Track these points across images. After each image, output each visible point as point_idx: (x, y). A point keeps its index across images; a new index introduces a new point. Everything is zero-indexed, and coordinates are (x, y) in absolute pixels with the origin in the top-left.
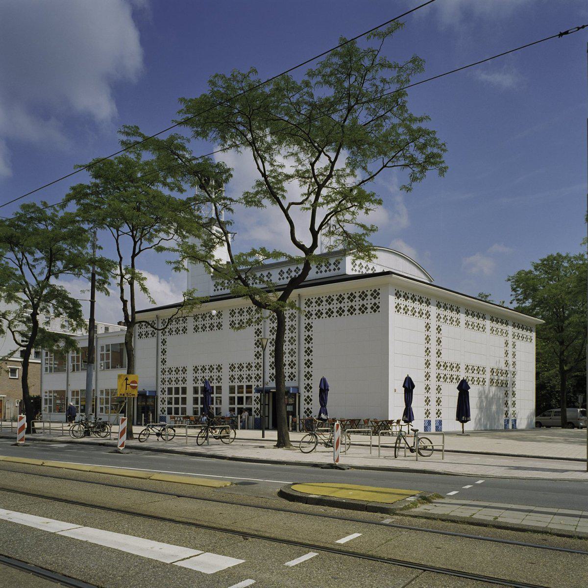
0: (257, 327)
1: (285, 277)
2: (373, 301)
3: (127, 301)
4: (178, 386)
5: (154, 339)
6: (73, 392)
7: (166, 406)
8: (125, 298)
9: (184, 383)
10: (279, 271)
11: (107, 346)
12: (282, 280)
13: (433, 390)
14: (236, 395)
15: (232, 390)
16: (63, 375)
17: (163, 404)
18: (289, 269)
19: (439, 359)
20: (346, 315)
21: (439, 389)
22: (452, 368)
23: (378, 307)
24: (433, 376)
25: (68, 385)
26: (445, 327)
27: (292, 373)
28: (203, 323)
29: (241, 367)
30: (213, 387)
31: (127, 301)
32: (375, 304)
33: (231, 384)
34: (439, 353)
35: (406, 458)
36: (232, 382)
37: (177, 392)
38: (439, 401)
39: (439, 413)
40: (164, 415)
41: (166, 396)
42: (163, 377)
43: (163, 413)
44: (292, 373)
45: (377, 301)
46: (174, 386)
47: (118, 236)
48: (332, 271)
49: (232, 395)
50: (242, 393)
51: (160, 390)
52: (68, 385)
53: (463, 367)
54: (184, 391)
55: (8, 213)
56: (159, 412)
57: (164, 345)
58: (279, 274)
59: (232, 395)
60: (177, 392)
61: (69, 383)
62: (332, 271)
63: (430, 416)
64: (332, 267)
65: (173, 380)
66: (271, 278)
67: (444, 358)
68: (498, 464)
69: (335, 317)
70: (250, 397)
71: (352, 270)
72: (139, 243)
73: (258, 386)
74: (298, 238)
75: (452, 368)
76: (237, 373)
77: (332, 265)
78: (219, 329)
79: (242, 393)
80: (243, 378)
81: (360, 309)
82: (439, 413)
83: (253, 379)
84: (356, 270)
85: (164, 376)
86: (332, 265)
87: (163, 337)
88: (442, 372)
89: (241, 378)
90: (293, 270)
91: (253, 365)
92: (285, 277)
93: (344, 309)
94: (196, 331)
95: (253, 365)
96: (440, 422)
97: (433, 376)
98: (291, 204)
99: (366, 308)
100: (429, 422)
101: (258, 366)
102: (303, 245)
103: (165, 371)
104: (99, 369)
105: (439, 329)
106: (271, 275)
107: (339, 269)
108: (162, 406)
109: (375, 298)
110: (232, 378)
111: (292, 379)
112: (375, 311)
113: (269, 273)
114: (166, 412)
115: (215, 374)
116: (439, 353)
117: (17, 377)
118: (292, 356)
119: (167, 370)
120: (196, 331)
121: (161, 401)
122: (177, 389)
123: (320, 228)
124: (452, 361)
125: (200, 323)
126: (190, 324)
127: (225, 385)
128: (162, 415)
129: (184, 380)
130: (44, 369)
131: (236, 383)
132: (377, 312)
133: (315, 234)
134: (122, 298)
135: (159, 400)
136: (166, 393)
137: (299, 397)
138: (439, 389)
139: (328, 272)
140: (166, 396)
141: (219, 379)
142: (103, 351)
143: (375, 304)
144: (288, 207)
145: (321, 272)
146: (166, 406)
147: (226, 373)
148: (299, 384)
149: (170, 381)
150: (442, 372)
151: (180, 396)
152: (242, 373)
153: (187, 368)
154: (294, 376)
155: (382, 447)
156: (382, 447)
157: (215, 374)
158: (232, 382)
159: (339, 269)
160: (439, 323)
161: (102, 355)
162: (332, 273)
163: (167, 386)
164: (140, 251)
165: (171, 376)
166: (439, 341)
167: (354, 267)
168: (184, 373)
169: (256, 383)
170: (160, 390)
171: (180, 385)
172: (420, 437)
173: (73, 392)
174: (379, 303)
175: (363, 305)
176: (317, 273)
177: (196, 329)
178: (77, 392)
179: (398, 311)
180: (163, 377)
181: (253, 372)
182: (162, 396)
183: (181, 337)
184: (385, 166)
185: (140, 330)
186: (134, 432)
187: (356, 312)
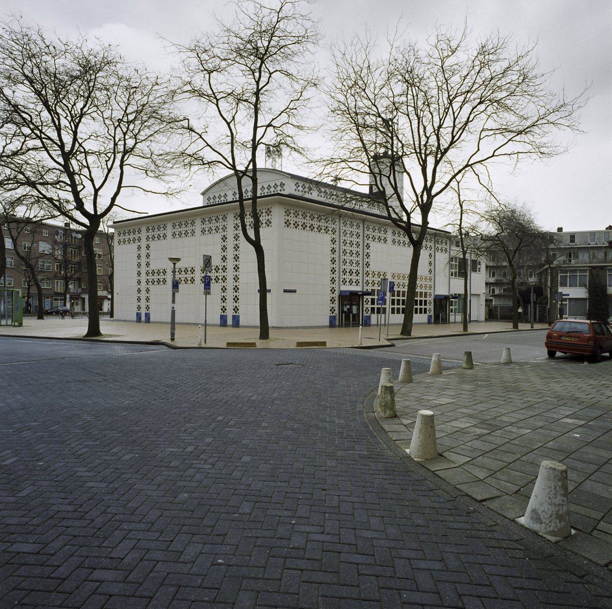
21: (148, 291)
28: (153, 233)
34: (148, 264)
41: (428, 307)
42: (358, 278)
66: (227, 198)
67: (153, 267)
68: (477, 336)
71: (296, 190)
78: (268, 226)
82: (148, 308)
84: (299, 190)
91: (220, 268)
95: (220, 268)
103: (222, 279)
106: (284, 185)
107: (284, 190)
116: (148, 264)
122: (426, 293)
124: (399, 248)
126: (169, 231)
136: (370, 303)
138: (148, 291)
140: (428, 307)
150: (151, 277)
151: (396, 306)
165: (153, 277)
166: (148, 256)
167: (297, 188)
168: (224, 282)
172: (383, 322)
180: (358, 278)
183: (162, 242)
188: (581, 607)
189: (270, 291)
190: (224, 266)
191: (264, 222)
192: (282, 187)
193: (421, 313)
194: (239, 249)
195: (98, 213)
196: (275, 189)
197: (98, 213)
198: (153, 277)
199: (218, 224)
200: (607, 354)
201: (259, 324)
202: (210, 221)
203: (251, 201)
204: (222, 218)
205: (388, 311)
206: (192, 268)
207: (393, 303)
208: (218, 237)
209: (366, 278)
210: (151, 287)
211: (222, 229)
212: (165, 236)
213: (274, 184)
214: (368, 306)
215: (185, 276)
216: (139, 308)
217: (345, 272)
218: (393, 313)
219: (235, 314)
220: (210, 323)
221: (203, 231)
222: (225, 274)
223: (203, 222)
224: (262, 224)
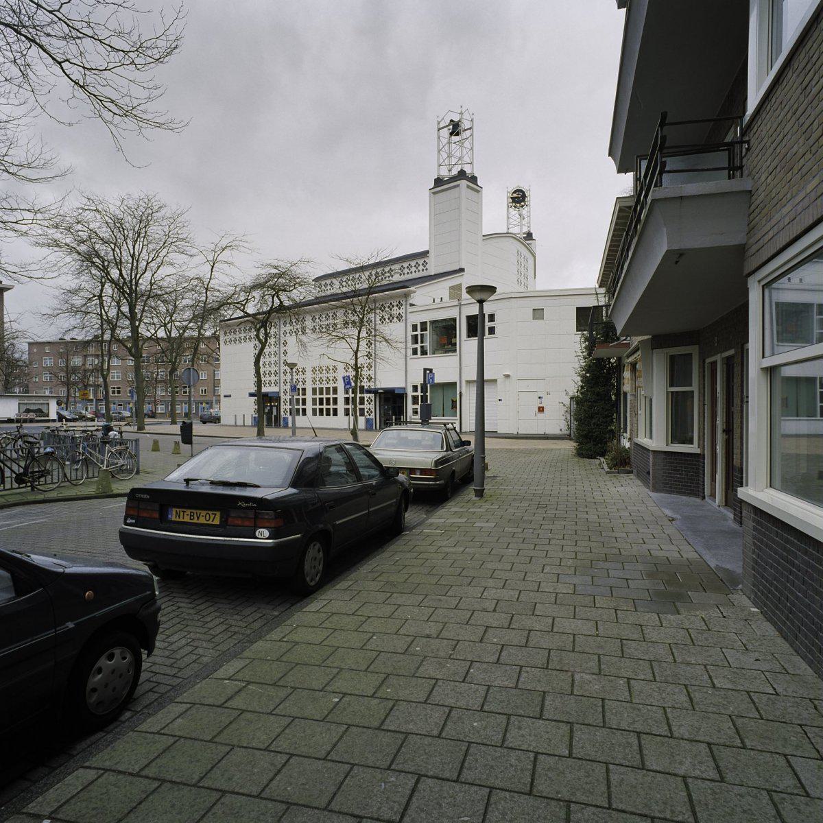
1: (421, 270)
5: (403, 324)
7: (288, 407)
9: (335, 383)
11: (423, 324)
14: (318, 396)
15: (314, 390)
30: (299, 389)
33: (314, 386)
37: (328, 393)
43: (370, 415)
46: (324, 386)
48: (413, 273)
51: (282, 391)
55: (45, 305)
62: (413, 273)
64: (421, 268)
77: (406, 269)
86: (406, 269)
89: (321, 381)
90: (421, 264)
92: (421, 270)
113: (425, 261)
122: (328, 389)
130: (410, 352)
131: (318, 386)
135: (282, 401)
141: (304, 382)
142: (416, 331)
147: (309, 376)
159: (427, 269)
162: (422, 274)
165: (270, 379)
170: (282, 391)
171: (331, 385)
182: (285, 397)
186: (180, 436)
188: (380, 820)
189: (251, 395)
192: (425, 266)
193: (328, 414)
196: (417, 268)
198: (270, 379)
201: (180, 433)
202: (390, 308)
205: (309, 412)
206: (304, 369)
207: (314, 403)
209: (277, 378)
213: (407, 265)
214: (368, 406)
215: (327, 375)
217: (276, 373)
218: (314, 413)
220: (502, 430)
222: (314, 376)
223: (314, 319)
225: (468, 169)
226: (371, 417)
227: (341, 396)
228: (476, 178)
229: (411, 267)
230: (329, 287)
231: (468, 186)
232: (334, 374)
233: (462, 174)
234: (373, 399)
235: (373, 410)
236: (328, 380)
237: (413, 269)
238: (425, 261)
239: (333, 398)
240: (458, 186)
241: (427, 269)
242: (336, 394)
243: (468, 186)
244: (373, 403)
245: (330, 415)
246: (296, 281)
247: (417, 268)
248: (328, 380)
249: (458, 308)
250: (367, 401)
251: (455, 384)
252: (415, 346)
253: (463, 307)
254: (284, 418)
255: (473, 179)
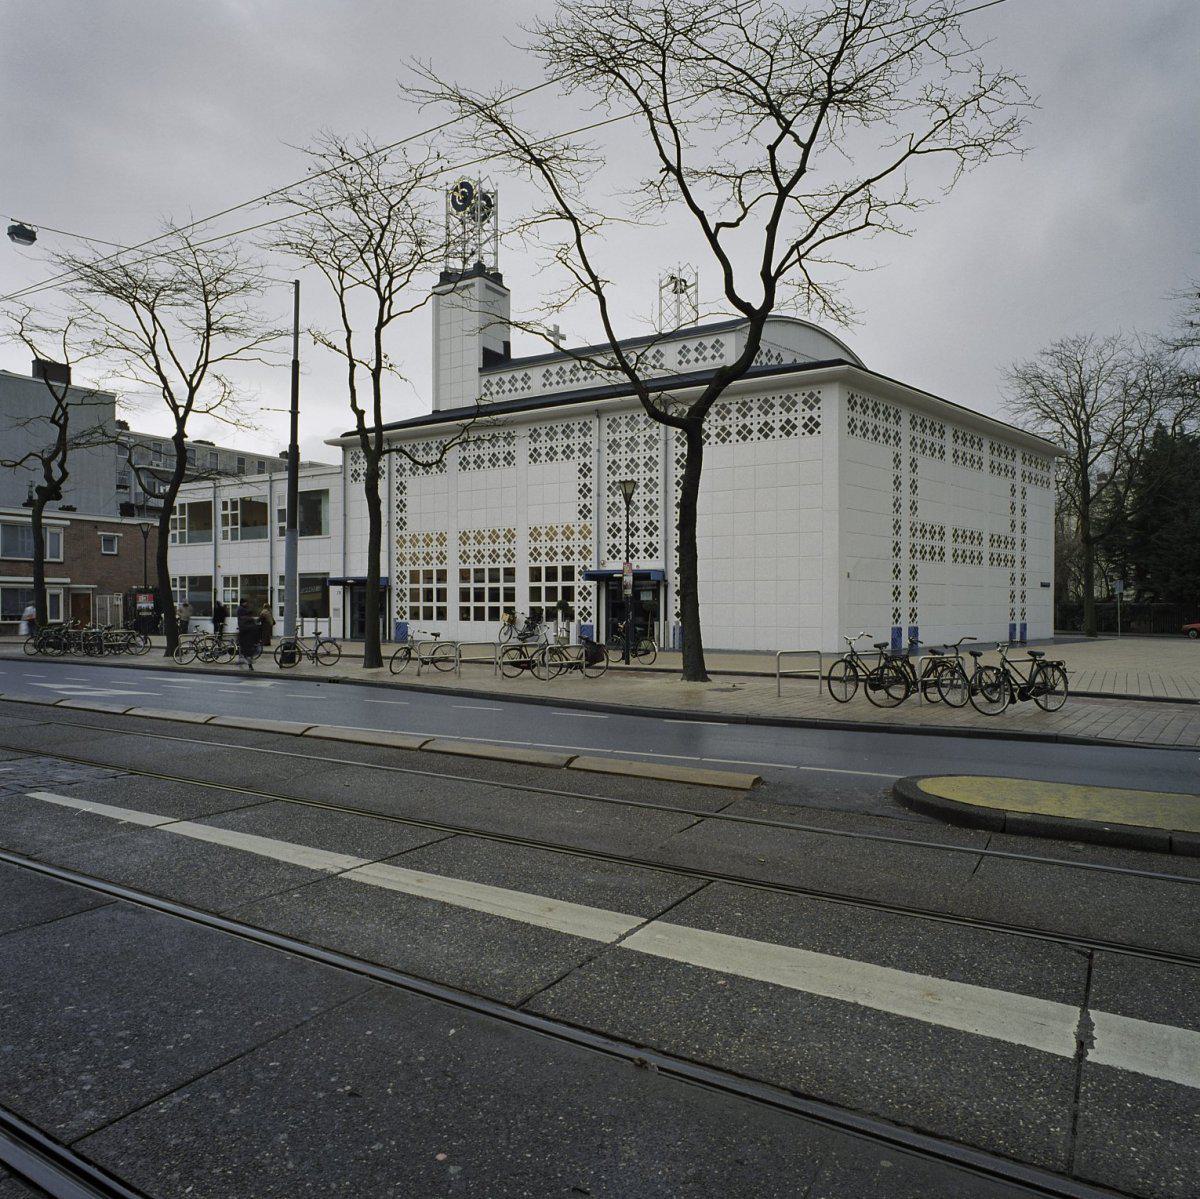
0: (582, 460)
2: (808, 414)
3: (363, 412)
4: (429, 568)
6: (226, 580)
7: (407, 604)
8: (360, 406)
9: (441, 563)
10: (510, 376)
12: (513, 392)
13: (905, 574)
16: (207, 549)
17: (402, 600)
18: (513, 377)
19: (914, 519)
20: (777, 437)
22: (933, 534)
23: (817, 425)
24: (905, 548)
25: (216, 567)
26: (923, 461)
27: (651, 545)
29: (551, 534)
31: (363, 412)
32: (811, 419)
33: (463, 566)
35: (526, 684)
36: (465, 562)
37: (494, 578)
38: (913, 594)
39: (913, 615)
40: (404, 620)
43: (402, 617)
44: (651, 545)
45: (815, 413)
46: (421, 567)
47: (343, 289)
48: (554, 385)
49: (536, 584)
50: (498, 581)
52: (216, 567)
53: (949, 532)
54: (510, 573)
56: (395, 615)
57: (401, 493)
58: (544, 376)
59: (536, 584)
60: (494, 578)
61: (219, 563)
63: (917, 619)
64: (519, 385)
65: (486, 554)
69: (734, 442)
70: (571, 589)
72: (388, 302)
73: (585, 567)
74: (739, 293)
75: (933, 534)
76: (543, 545)
79: (498, 581)
80: (431, 559)
81: (782, 428)
82: (913, 615)
83: (576, 556)
85: (403, 550)
86: (555, 376)
87: (399, 480)
88: (919, 541)
90: (554, 373)
93: (773, 425)
94: (464, 468)
96: (916, 629)
97: (905, 548)
98: (719, 226)
99: (794, 427)
100: (900, 630)
101: (585, 533)
102: (749, 304)
104: (220, 540)
105: (914, 465)
106: (529, 378)
108: (400, 604)
109: (811, 408)
110: (535, 554)
111: (651, 556)
112: (811, 431)
113: (526, 375)
114: (408, 615)
115: (502, 546)
117: (115, 552)
118: (651, 513)
119: (408, 538)
120: (464, 468)
121: (398, 595)
123: (779, 272)
125: (501, 450)
126: (522, 447)
127: (522, 566)
128: (399, 620)
129: (442, 557)
132: (816, 433)
133: (769, 281)
134: (354, 406)
135: (394, 593)
137: (666, 587)
138: (913, 572)
139: (701, 362)
140: (407, 586)
143: (811, 419)
144: (717, 230)
145: (551, 384)
146: (407, 604)
148: (389, 573)
149: (414, 559)
150: (919, 541)
151: (502, 585)
152: (430, 550)
153: (447, 536)
154: (656, 550)
155: (816, 678)
156: (816, 678)
157: (501, 546)
158: (465, 562)
159: (529, 388)
160: (914, 455)
161: (225, 517)
163: (407, 568)
164: (390, 317)
169: (582, 563)
173: (226, 580)
174: (819, 416)
175: (788, 422)
176: (544, 385)
177: (534, 456)
178: (235, 579)
179: (853, 432)
181: (576, 543)
182: (400, 586)
184: (912, 152)
185: (354, 467)
186: (383, 654)
187: (774, 433)
190: (441, 553)
191: (713, 432)
194: (579, 509)
195: (784, 186)
197: (784, 186)
199: (496, 450)
200: (638, 629)
203: (358, 436)
204: (424, 449)
208: (572, 467)
210: (921, 566)
211: (475, 462)
212: (509, 459)
216: (897, 615)
219: (583, 623)
220: (1039, 636)
221: (534, 456)
223: (534, 436)
224: (708, 436)
225: (488, 262)
226: (588, 623)
227: (453, 586)
228: (501, 276)
229: (516, 380)
230: (709, 352)
231: (488, 287)
232: (537, 545)
233: (480, 269)
234: (594, 590)
235: (594, 611)
236: (428, 558)
237: (507, 387)
238: (526, 375)
239: (438, 590)
240: (473, 285)
241: (529, 388)
242: (445, 581)
243: (488, 287)
244: (594, 597)
245: (418, 618)
246: (128, 429)
247: (500, 387)
248: (428, 558)
249: (268, 483)
250: (405, 595)
251: (265, 577)
252: (225, 528)
253: (274, 484)
254: (399, 626)
255: (497, 278)
